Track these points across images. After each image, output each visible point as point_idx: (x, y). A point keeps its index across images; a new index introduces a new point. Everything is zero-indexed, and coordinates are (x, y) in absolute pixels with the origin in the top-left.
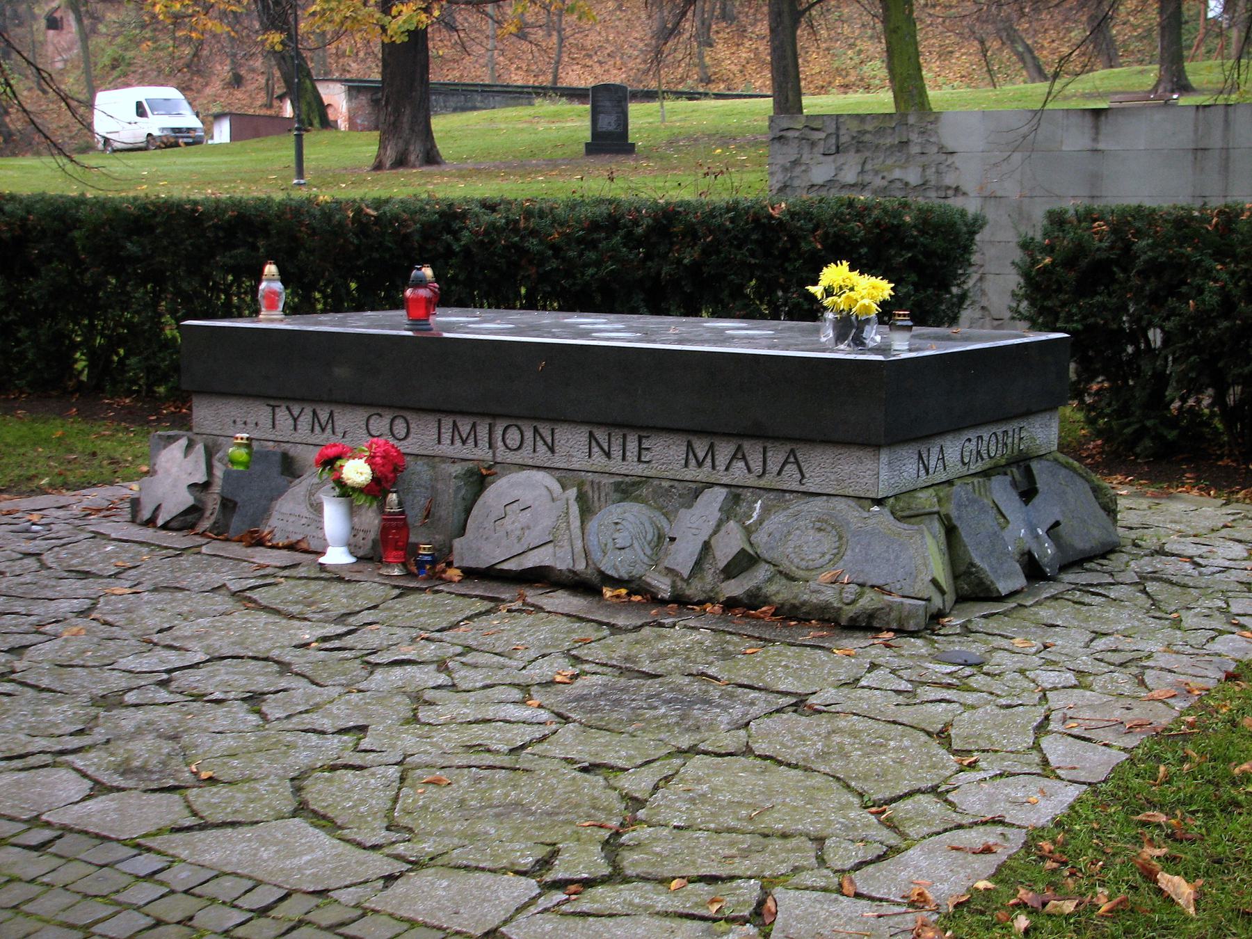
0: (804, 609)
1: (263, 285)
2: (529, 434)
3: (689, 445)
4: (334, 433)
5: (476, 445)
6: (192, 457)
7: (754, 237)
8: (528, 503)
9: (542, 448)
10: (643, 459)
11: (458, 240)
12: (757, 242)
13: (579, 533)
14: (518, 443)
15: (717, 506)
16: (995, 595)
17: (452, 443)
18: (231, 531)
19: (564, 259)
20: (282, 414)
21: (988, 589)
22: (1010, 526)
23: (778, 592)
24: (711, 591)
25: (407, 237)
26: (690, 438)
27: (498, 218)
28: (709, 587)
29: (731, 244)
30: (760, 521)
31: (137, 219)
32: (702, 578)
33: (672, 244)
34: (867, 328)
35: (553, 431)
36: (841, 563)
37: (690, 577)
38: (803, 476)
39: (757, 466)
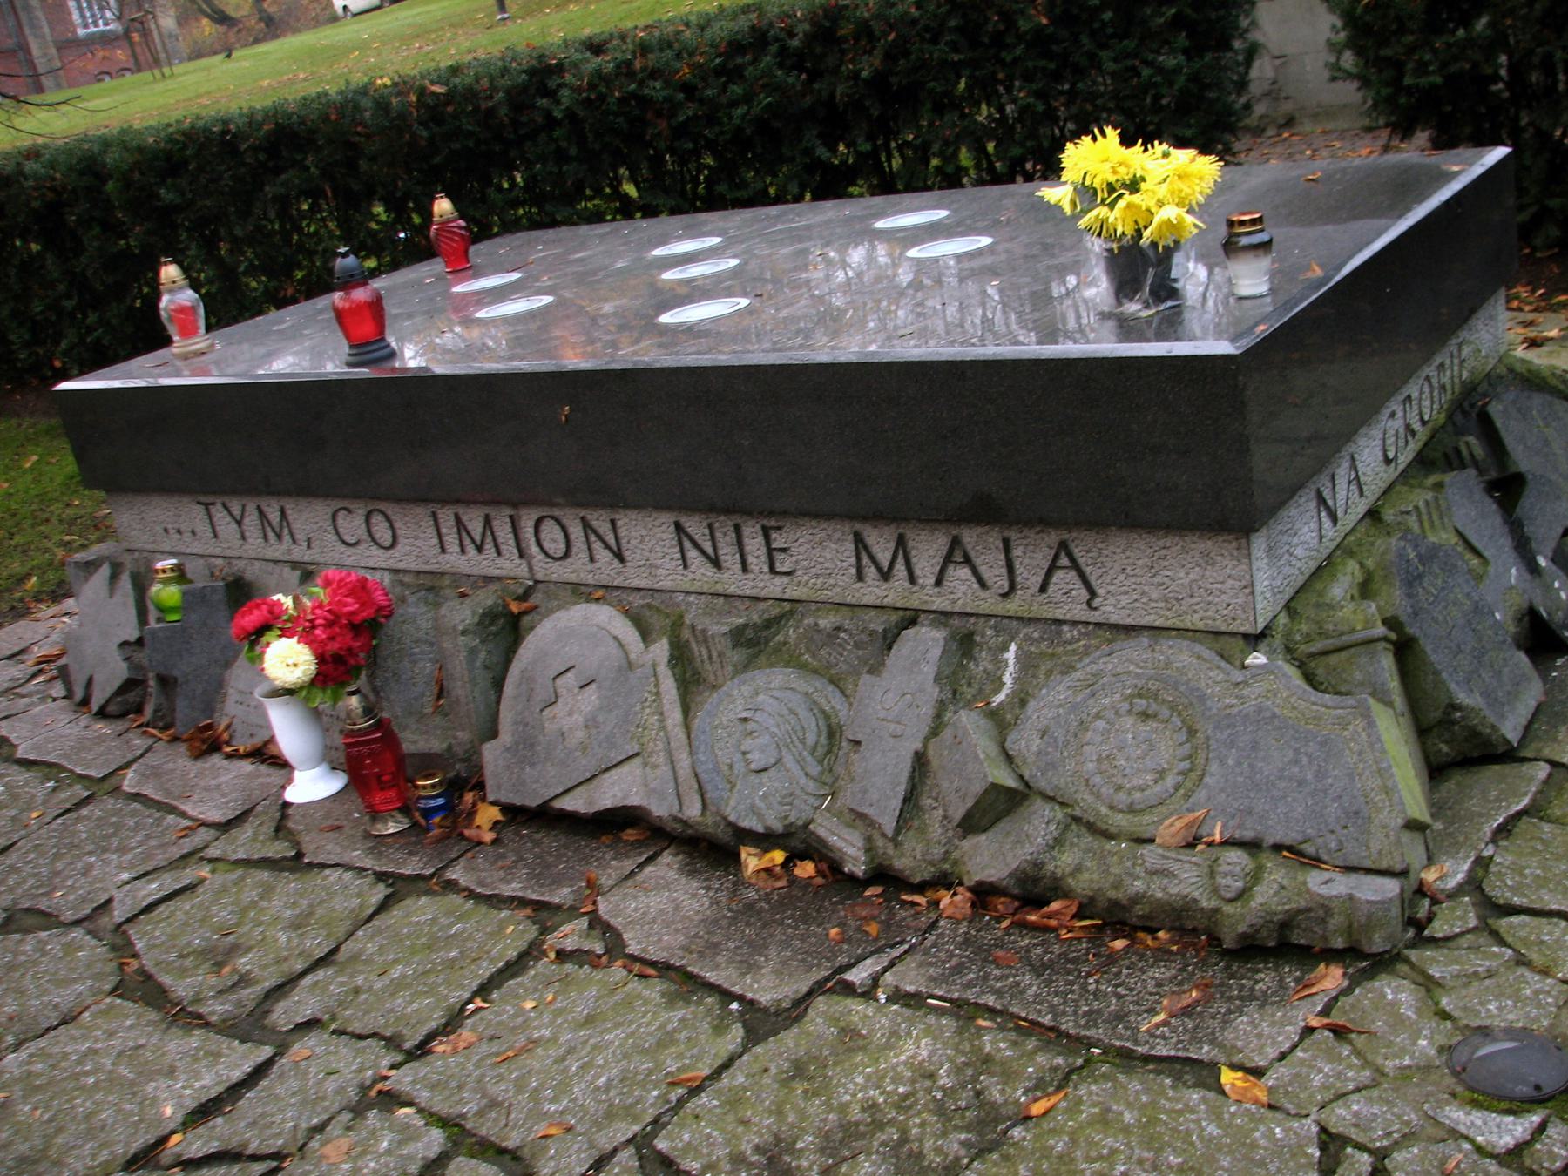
0: (1139, 910)
1: (165, 301)
2: (576, 531)
3: (859, 540)
4: (294, 541)
5: (499, 553)
6: (118, 597)
7: (953, 23)
8: (596, 671)
9: (603, 555)
10: (779, 568)
11: (558, 102)
12: (957, 29)
13: (682, 735)
14: (562, 546)
15: (929, 670)
16: (1501, 750)
17: (463, 551)
18: (178, 723)
19: (701, 101)
20: (219, 513)
21: (1487, 742)
22: (1491, 569)
23: (1078, 869)
24: (945, 858)
25: (491, 112)
26: (858, 526)
27: (606, 62)
28: (938, 852)
29: (923, 39)
30: (1021, 699)
31: (169, 156)
32: (922, 830)
33: (843, 52)
34: (1178, 258)
35: (613, 522)
36: (1201, 794)
37: (898, 830)
38: (1093, 594)
39: (996, 576)
